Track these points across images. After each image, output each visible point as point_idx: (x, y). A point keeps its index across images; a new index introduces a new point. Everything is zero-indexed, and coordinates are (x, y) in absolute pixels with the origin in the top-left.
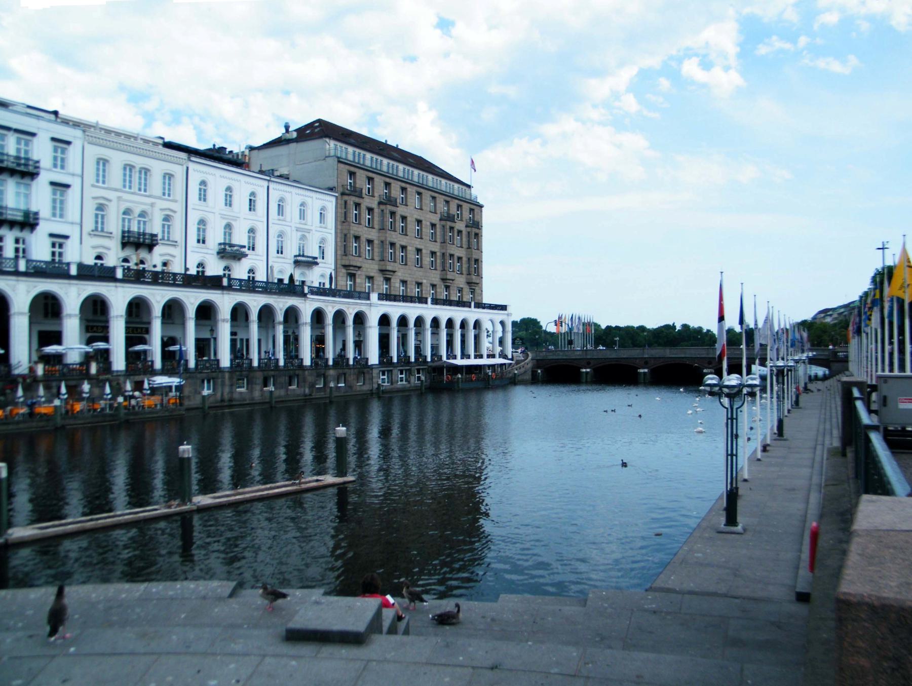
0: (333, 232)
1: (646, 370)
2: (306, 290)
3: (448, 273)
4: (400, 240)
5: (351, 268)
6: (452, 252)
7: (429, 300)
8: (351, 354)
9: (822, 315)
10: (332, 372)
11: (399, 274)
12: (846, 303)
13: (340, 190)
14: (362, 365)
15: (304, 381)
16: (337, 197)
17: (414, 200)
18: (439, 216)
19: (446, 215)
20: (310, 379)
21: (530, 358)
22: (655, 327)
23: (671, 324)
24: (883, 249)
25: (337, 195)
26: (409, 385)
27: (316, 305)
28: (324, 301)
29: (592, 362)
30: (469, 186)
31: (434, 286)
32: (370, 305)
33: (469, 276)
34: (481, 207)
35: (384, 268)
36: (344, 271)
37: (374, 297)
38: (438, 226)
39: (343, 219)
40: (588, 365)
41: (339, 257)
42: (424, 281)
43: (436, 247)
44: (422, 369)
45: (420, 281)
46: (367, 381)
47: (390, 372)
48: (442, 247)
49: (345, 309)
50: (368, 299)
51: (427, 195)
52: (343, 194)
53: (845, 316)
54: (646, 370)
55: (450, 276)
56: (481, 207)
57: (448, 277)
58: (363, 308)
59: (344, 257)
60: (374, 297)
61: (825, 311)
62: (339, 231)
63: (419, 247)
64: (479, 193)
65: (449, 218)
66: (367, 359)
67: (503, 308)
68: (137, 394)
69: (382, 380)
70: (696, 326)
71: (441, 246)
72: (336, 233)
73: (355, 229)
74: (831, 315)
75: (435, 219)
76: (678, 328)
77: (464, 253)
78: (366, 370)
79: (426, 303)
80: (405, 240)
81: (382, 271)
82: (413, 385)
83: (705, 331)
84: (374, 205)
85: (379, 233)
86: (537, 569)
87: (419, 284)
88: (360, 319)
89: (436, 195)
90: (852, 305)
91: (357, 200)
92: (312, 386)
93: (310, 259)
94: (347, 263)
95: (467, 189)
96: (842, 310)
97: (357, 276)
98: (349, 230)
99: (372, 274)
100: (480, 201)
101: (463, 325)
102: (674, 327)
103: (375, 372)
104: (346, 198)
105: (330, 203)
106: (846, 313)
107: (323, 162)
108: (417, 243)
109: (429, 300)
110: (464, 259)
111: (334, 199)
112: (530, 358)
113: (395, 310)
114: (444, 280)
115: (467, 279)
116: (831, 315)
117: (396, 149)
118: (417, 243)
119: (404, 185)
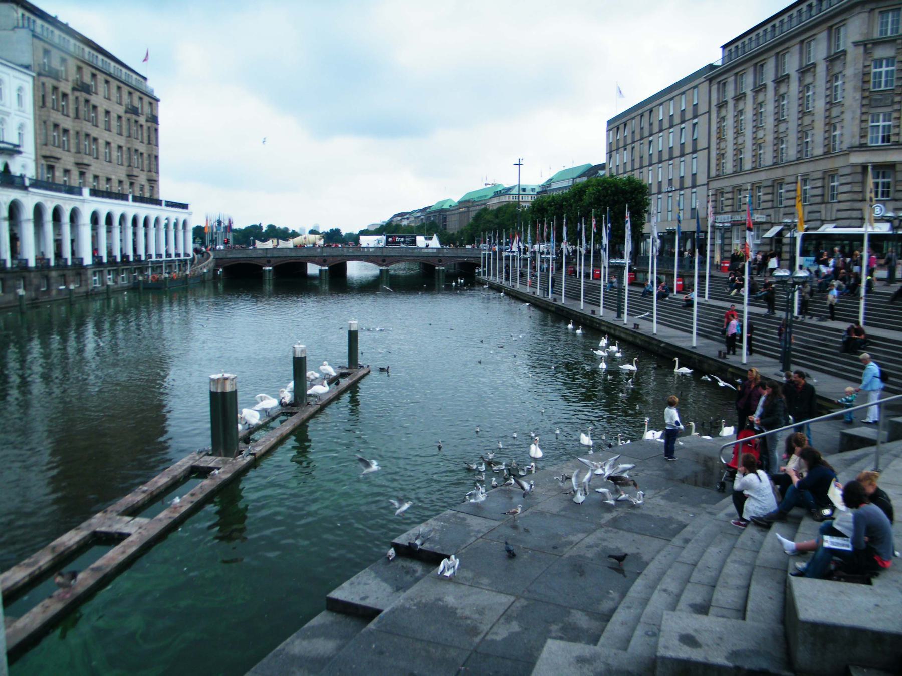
0: (31, 117)
1: (271, 268)
2: (27, 183)
3: (134, 169)
4: (94, 133)
5: (52, 160)
6: (137, 147)
7: (130, 197)
8: (67, 254)
9: (399, 218)
10: (54, 274)
11: (92, 168)
12: (421, 208)
13: (37, 69)
14: (78, 264)
15: (31, 285)
16: (33, 77)
17: (102, 88)
18: (124, 107)
19: (130, 107)
20: (35, 281)
21: (212, 257)
22: (243, 228)
23: (258, 224)
24: (519, 164)
25: (34, 74)
26: (116, 287)
27: (37, 199)
28: (44, 196)
29: (272, 260)
30: (145, 79)
31: (120, 182)
32: (83, 201)
33: (149, 174)
34: (157, 100)
35: (80, 161)
36: (43, 162)
37: (86, 192)
38: (124, 119)
39: (41, 104)
40: (268, 263)
41: (39, 146)
42: (113, 177)
43: (122, 141)
44: (127, 269)
45: (110, 176)
46: (83, 283)
47: (101, 272)
48: (127, 142)
49: (44, 203)
50: (80, 194)
51: (114, 84)
52: (39, 74)
53: (422, 219)
54: (271, 268)
55: (136, 172)
56: (157, 100)
57: (135, 173)
58: (77, 204)
59: (44, 147)
60: (86, 192)
61: (402, 215)
62: (37, 117)
63: (109, 140)
64: (154, 85)
65: (134, 111)
66: (82, 259)
67: (184, 206)
68: (875, 266)
69: (94, 281)
70: (282, 227)
71: (126, 140)
72: (35, 118)
73: (57, 117)
74: (408, 219)
75: (121, 110)
76: (264, 229)
77: (145, 148)
78: (82, 271)
79: (127, 200)
80: (97, 132)
81: (78, 164)
82: (119, 286)
83: (290, 232)
84: (68, 90)
85: (74, 122)
86: (896, 390)
87: (109, 180)
88: (74, 215)
89: (121, 85)
90: (428, 210)
91: (55, 83)
92: (37, 289)
93: (11, 147)
94: (48, 154)
95: (143, 81)
96: (419, 214)
97: (56, 169)
98: (49, 116)
99: (68, 167)
100: (157, 94)
101: (57, 214)
102: (260, 227)
103: (90, 272)
104: (43, 79)
105: (26, 83)
106: (423, 217)
107: (12, 32)
108: (106, 135)
109: (130, 197)
110: (145, 155)
111: (30, 80)
112: (212, 257)
113: (104, 206)
114: (129, 176)
115: (147, 176)
116: (408, 219)
117: (66, 25)
118: (106, 135)
119: (94, 71)
